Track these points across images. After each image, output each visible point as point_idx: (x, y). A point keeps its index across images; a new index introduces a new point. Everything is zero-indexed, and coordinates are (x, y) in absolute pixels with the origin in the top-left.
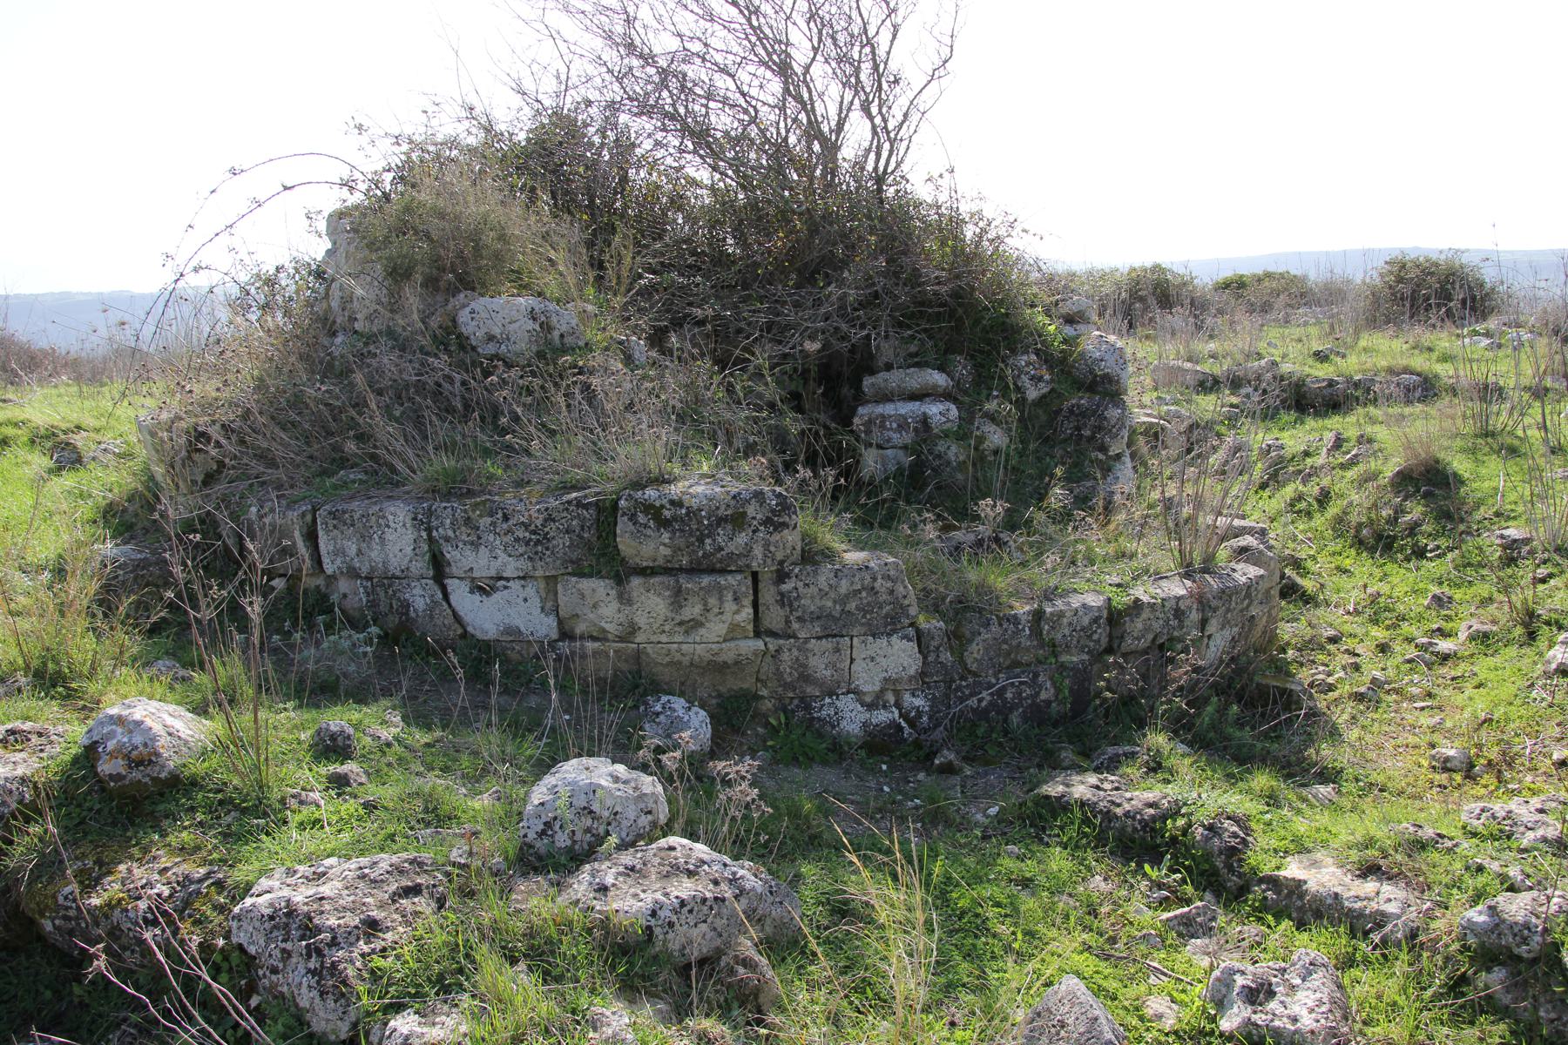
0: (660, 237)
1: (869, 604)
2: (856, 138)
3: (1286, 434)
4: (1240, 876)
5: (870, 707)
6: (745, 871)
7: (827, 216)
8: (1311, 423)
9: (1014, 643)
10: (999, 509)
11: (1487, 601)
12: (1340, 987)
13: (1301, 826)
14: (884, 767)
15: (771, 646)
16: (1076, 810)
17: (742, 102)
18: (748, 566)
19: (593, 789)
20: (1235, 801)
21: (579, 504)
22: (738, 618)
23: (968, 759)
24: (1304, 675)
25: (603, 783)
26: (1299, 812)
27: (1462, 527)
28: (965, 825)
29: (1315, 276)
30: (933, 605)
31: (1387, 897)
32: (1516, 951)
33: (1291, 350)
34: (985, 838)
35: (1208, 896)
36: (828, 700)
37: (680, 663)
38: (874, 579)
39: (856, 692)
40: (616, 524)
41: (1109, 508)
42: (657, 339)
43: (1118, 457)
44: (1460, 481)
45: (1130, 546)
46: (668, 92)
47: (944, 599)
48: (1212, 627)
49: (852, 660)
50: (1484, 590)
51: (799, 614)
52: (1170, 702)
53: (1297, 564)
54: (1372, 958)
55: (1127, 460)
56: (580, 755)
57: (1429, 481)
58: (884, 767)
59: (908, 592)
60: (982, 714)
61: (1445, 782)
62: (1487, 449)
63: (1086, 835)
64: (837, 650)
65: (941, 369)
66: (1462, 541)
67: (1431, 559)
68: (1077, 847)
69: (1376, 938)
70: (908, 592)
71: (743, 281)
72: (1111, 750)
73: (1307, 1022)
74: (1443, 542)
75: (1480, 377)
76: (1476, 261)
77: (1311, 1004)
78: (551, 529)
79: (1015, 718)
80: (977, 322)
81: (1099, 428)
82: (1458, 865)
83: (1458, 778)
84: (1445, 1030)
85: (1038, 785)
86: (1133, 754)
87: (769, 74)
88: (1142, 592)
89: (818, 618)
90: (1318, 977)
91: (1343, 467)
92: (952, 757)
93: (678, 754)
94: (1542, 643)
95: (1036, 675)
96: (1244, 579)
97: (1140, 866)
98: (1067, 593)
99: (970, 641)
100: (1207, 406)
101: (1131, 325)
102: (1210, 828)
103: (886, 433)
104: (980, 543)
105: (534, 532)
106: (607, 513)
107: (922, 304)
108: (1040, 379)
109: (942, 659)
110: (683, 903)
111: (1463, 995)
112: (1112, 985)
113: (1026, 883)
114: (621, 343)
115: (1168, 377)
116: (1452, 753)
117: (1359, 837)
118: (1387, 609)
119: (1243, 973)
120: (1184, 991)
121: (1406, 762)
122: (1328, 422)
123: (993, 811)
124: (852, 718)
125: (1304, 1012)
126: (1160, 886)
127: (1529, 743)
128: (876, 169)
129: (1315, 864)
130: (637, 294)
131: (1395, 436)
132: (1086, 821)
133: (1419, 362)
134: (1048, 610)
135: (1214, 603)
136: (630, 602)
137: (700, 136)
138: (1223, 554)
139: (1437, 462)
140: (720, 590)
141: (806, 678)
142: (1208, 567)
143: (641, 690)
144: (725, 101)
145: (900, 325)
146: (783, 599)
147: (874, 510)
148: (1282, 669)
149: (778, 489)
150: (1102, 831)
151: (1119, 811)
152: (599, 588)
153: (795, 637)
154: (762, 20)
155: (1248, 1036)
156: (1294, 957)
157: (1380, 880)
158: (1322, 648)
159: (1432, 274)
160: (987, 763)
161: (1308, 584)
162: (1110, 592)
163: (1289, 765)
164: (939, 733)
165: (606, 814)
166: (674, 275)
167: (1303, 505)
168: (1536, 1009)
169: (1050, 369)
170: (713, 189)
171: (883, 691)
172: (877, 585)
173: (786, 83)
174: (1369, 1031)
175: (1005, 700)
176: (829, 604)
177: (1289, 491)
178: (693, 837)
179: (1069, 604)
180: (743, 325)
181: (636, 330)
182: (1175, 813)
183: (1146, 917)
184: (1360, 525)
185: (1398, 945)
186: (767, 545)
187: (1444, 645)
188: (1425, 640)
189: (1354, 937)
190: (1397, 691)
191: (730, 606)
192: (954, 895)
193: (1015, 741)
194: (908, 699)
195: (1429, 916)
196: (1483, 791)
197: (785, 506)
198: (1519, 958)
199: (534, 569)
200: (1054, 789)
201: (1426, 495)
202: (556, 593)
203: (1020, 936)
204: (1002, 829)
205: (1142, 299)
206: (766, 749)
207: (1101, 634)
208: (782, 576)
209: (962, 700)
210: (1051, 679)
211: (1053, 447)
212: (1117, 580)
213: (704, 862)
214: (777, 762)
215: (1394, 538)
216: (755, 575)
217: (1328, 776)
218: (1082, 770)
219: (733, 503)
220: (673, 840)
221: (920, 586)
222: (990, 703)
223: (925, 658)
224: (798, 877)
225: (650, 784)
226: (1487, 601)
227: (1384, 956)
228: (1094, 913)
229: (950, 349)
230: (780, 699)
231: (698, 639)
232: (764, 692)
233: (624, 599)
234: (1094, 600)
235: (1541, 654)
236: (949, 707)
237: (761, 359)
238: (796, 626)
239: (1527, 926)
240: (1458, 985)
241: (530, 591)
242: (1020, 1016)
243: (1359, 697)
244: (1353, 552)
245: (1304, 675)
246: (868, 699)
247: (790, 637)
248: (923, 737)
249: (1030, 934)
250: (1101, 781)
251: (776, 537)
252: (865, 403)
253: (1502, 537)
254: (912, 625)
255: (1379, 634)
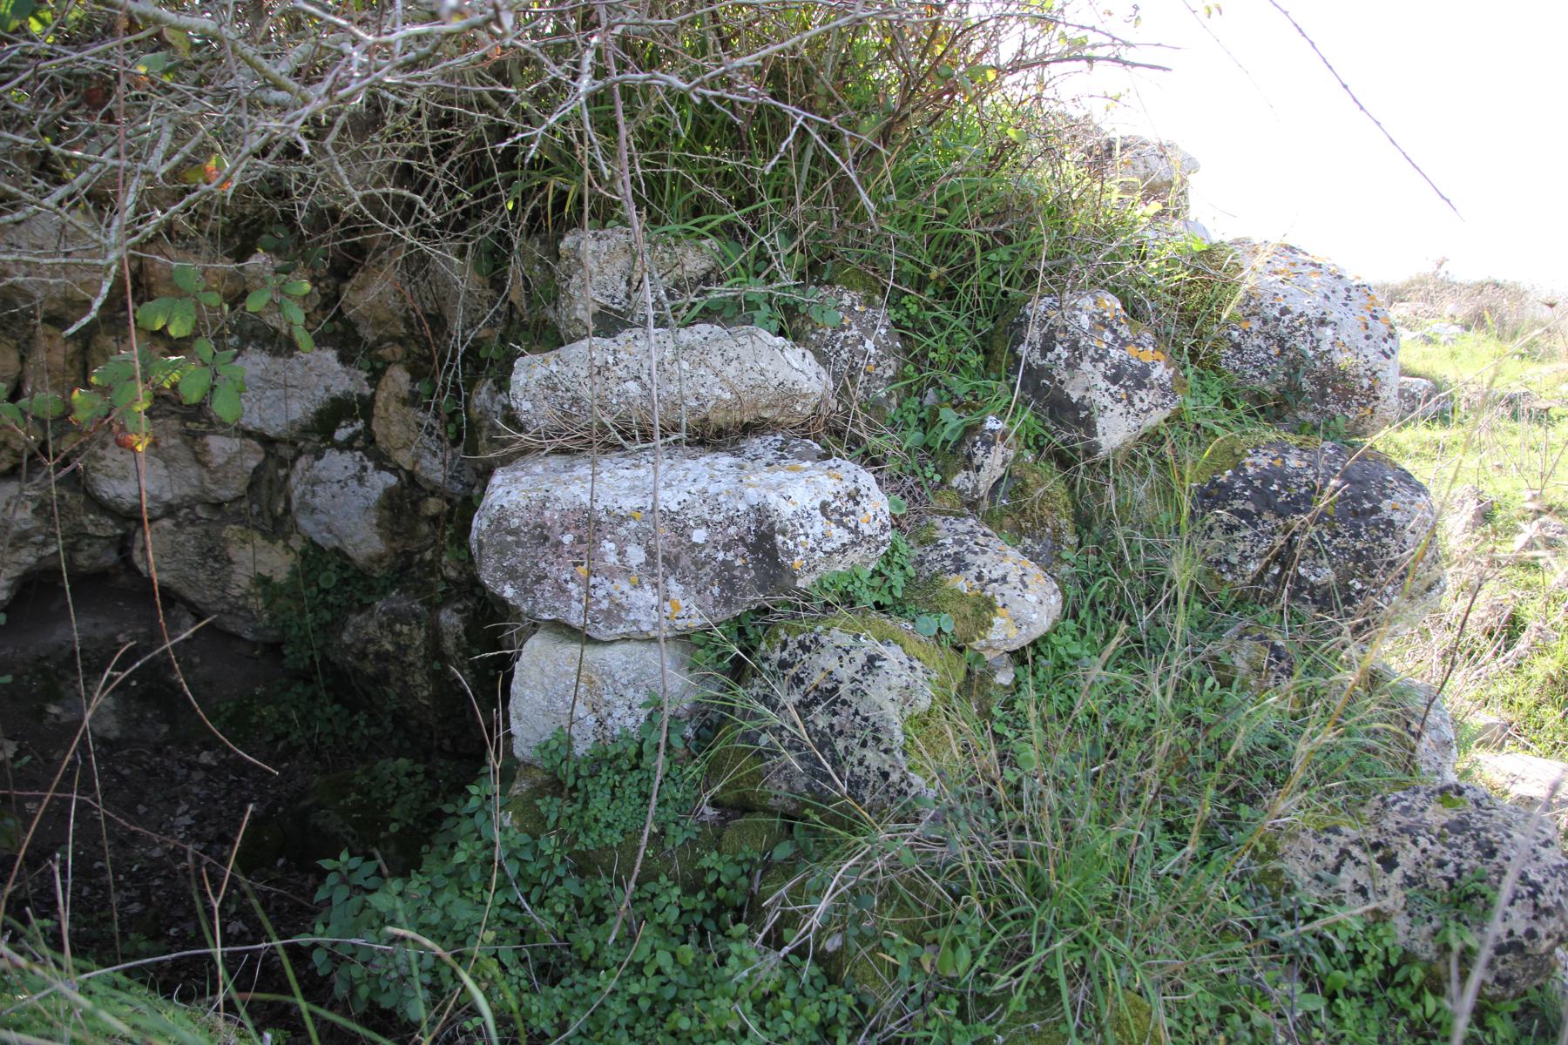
65: (791, 324)
108: (1141, 379)
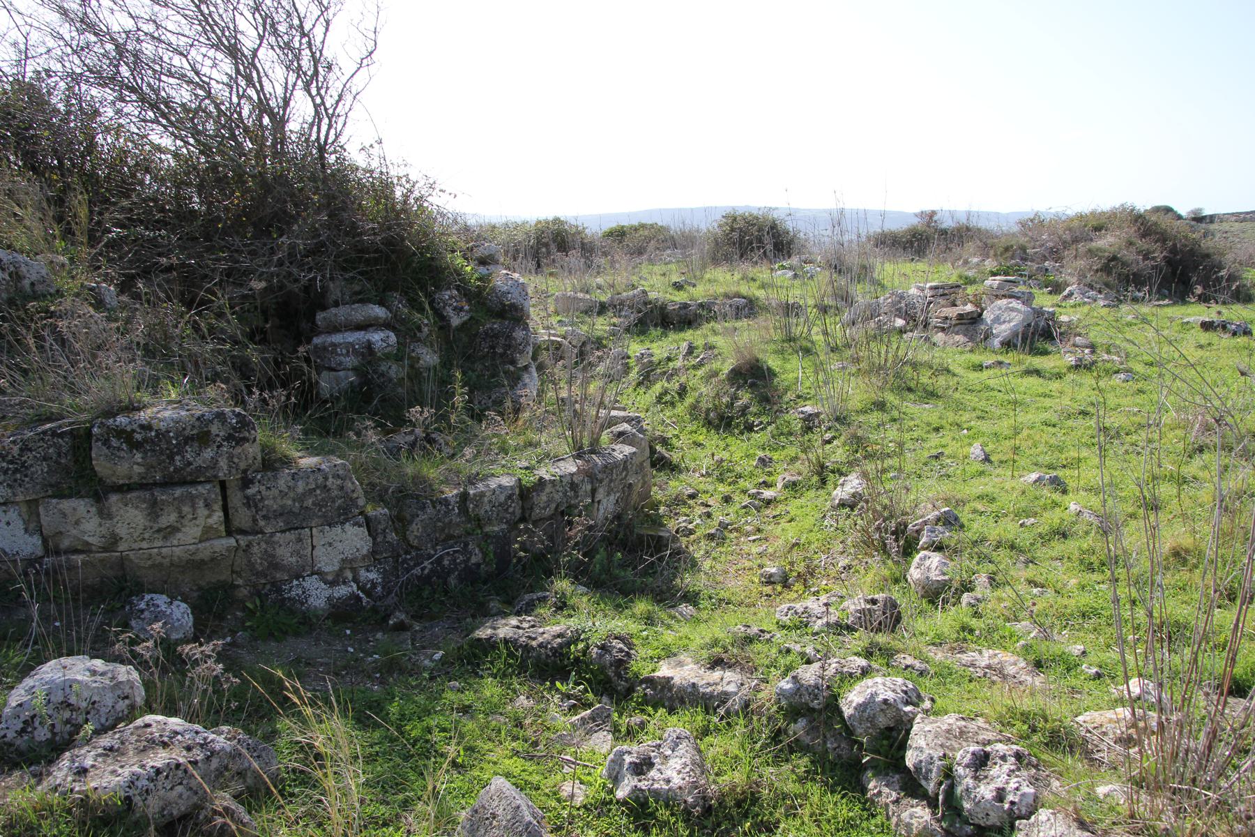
0: (128, 197)
1: (323, 499)
2: (301, 111)
3: (654, 345)
4: (627, 680)
5: (333, 584)
6: (221, 738)
7: (280, 179)
8: (672, 336)
9: (447, 520)
10: (426, 414)
11: (794, 459)
12: (700, 751)
13: (668, 637)
14: (348, 632)
15: (241, 542)
16: (502, 646)
17: (191, 74)
18: (216, 476)
19: (70, 684)
20: (622, 624)
21: (54, 433)
22: (210, 521)
23: (417, 617)
24: (672, 525)
25: (79, 678)
26: (669, 627)
27: (775, 408)
28: (415, 671)
29: (675, 226)
30: (378, 495)
31: (728, 681)
32: (811, 705)
33: (657, 281)
34: (432, 678)
35: (605, 699)
36: (295, 582)
37: (161, 564)
38: (326, 479)
39: (319, 573)
40: (91, 449)
41: (517, 410)
42: (126, 286)
43: (526, 368)
44: (772, 373)
45: (535, 437)
46: (124, 65)
47: (387, 491)
48: (600, 495)
49: (313, 547)
50: (792, 451)
51: (264, 513)
52: (570, 554)
53: (665, 442)
54: (721, 727)
55: (533, 370)
56: (61, 655)
57: (753, 375)
58: (348, 632)
59: (355, 486)
60: (424, 580)
61: (770, 592)
62: (790, 351)
63: (511, 665)
64: (300, 540)
65: (381, 303)
66: (777, 417)
67: (757, 432)
68: (504, 675)
69: (722, 711)
70: (355, 486)
71: (205, 232)
72: (527, 597)
73: (677, 781)
74: (765, 419)
75: (784, 300)
76: (783, 216)
77: (678, 767)
78: (28, 457)
79: (452, 581)
80: (408, 265)
81: (509, 346)
82: (774, 650)
83: (779, 588)
84: (771, 769)
85: (472, 631)
86: (545, 598)
87: (220, 56)
88: (545, 472)
89: (281, 515)
90: (683, 746)
91: (695, 367)
92: (403, 617)
93: (150, 644)
94: (830, 486)
95: (466, 545)
96: (621, 456)
97: (553, 683)
98: (485, 478)
99: (411, 522)
100: (601, 325)
101: (539, 266)
102: (603, 647)
103: (338, 358)
104: (413, 445)
105: (11, 462)
106: (81, 440)
107: (360, 251)
108: (461, 309)
109: (389, 538)
110: (158, 771)
111: (781, 742)
112: (535, 778)
113: (465, 710)
114: (92, 289)
115: (568, 305)
116: (773, 570)
117: (707, 640)
118: (729, 471)
119: (630, 753)
120: (589, 774)
121: (743, 581)
122: (682, 335)
123: (437, 657)
124: (318, 595)
125: (675, 774)
126: (569, 697)
127: (823, 557)
128: (318, 138)
129: (680, 664)
130: (106, 246)
131: (728, 343)
132: (511, 655)
133: (744, 289)
134: (471, 492)
135: (600, 476)
136: (110, 516)
137: (158, 105)
138: (605, 437)
139: (757, 360)
140: (192, 500)
141: (275, 565)
142: (595, 449)
143: (127, 591)
144: (182, 77)
145: (344, 269)
146: (249, 502)
147: (322, 419)
148: (657, 522)
149: (237, 410)
150: (523, 661)
151: (534, 643)
152: (80, 506)
153: (262, 533)
154: (212, 9)
155: (637, 800)
156: (666, 735)
157: (723, 669)
158: (685, 503)
159: (754, 225)
160: (432, 618)
161: (675, 457)
162: (520, 474)
163: (662, 592)
164: (391, 600)
165: (84, 704)
166: (140, 229)
167: (668, 398)
168: (825, 742)
169: (469, 301)
170: (176, 155)
171: (341, 570)
172: (329, 483)
173: (236, 65)
174: (720, 780)
175: (443, 567)
176: (290, 502)
177: (658, 388)
178: (171, 711)
179: (488, 486)
180: (207, 271)
181: (107, 278)
182: (576, 640)
183: (560, 719)
184: (708, 410)
185: (737, 714)
186: (230, 457)
187: (768, 494)
188: (755, 491)
189: (708, 713)
190: (737, 530)
191: (202, 512)
192: (408, 728)
193: (457, 596)
194: (363, 574)
195: (757, 690)
196: (795, 595)
197: (244, 423)
198: (813, 710)
199: (14, 495)
200: (483, 633)
201: (752, 386)
202: (38, 515)
203: (462, 753)
204: (445, 670)
205: (546, 245)
206: (245, 629)
207: (516, 507)
208: (246, 482)
209: (408, 570)
210: (479, 546)
211: (473, 363)
212: (526, 464)
213: (177, 733)
214: (256, 639)
215: (732, 418)
216: (223, 485)
217: (691, 598)
218: (505, 615)
219: (197, 424)
220: (149, 718)
221: (366, 482)
222: (431, 570)
223: (374, 539)
224: (275, 733)
225: (127, 673)
226: (794, 459)
227: (728, 724)
228: (519, 724)
229: (389, 287)
230: (254, 586)
231: (175, 542)
232: (240, 582)
233: (105, 514)
234: (507, 481)
235: (829, 494)
236: (398, 577)
237: (222, 300)
238: (262, 523)
239: (816, 687)
240: (776, 736)
241: (12, 514)
242: (463, 815)
243: (711, 537)
244: (704, 430)
245: (672, 525)
246: (330, 578)
247: (257, 533)
248: (378, 603)
249: (470, 749)
250: (521, 622)
251: (239, 450)
252: (319, 334)
253: (802, 412)
254: (361, 513)
255: (723, 489)
